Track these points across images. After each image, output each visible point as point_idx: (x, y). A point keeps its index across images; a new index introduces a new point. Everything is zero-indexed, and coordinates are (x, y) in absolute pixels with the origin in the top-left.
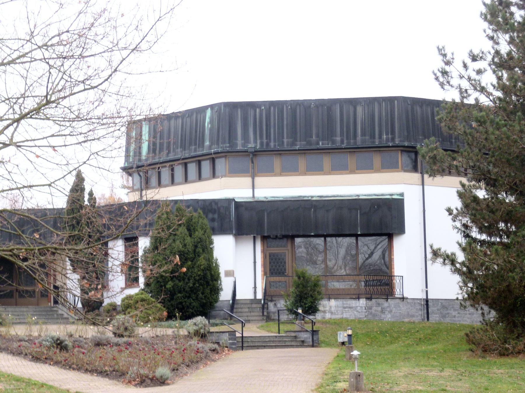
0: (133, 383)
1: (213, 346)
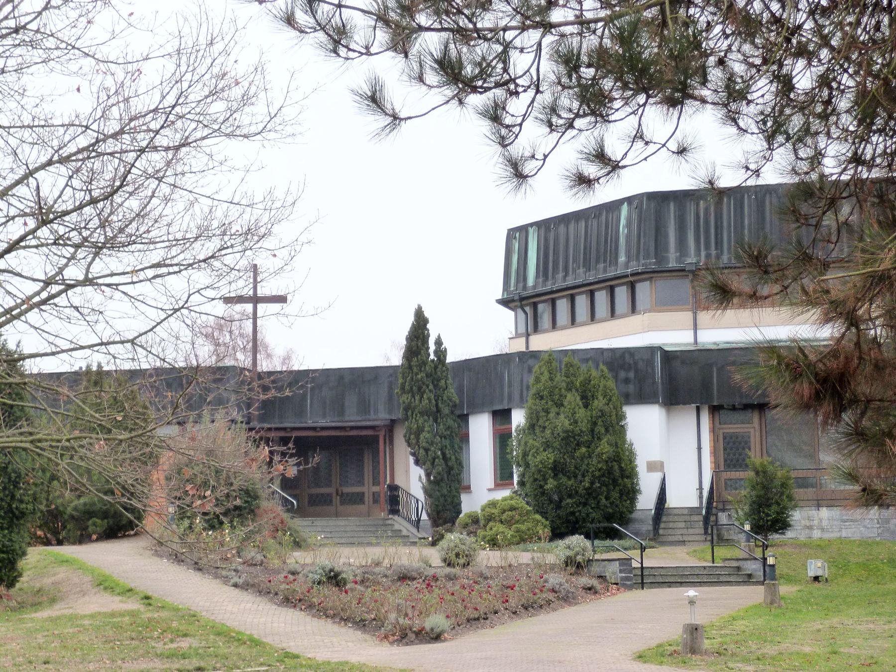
0: (391, 638)
1: (590, 581)
